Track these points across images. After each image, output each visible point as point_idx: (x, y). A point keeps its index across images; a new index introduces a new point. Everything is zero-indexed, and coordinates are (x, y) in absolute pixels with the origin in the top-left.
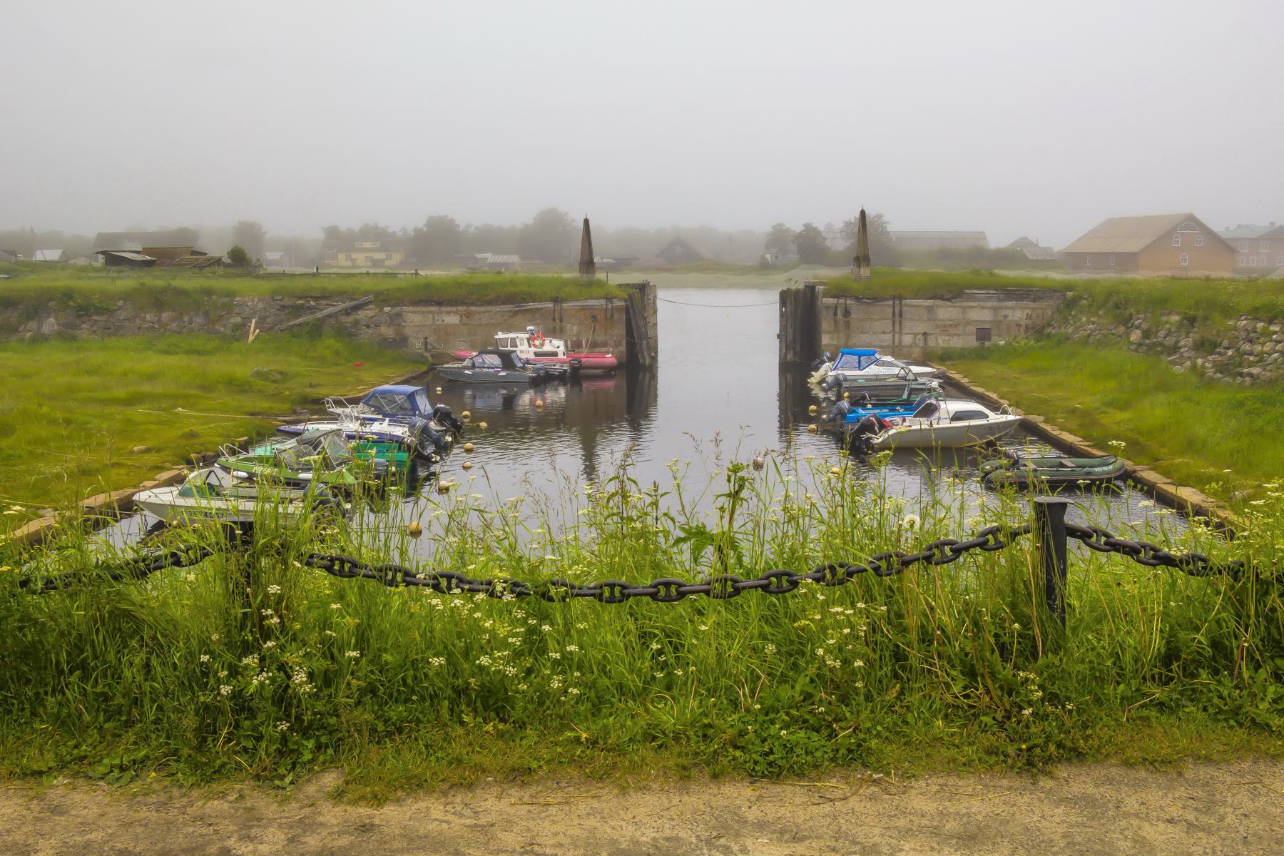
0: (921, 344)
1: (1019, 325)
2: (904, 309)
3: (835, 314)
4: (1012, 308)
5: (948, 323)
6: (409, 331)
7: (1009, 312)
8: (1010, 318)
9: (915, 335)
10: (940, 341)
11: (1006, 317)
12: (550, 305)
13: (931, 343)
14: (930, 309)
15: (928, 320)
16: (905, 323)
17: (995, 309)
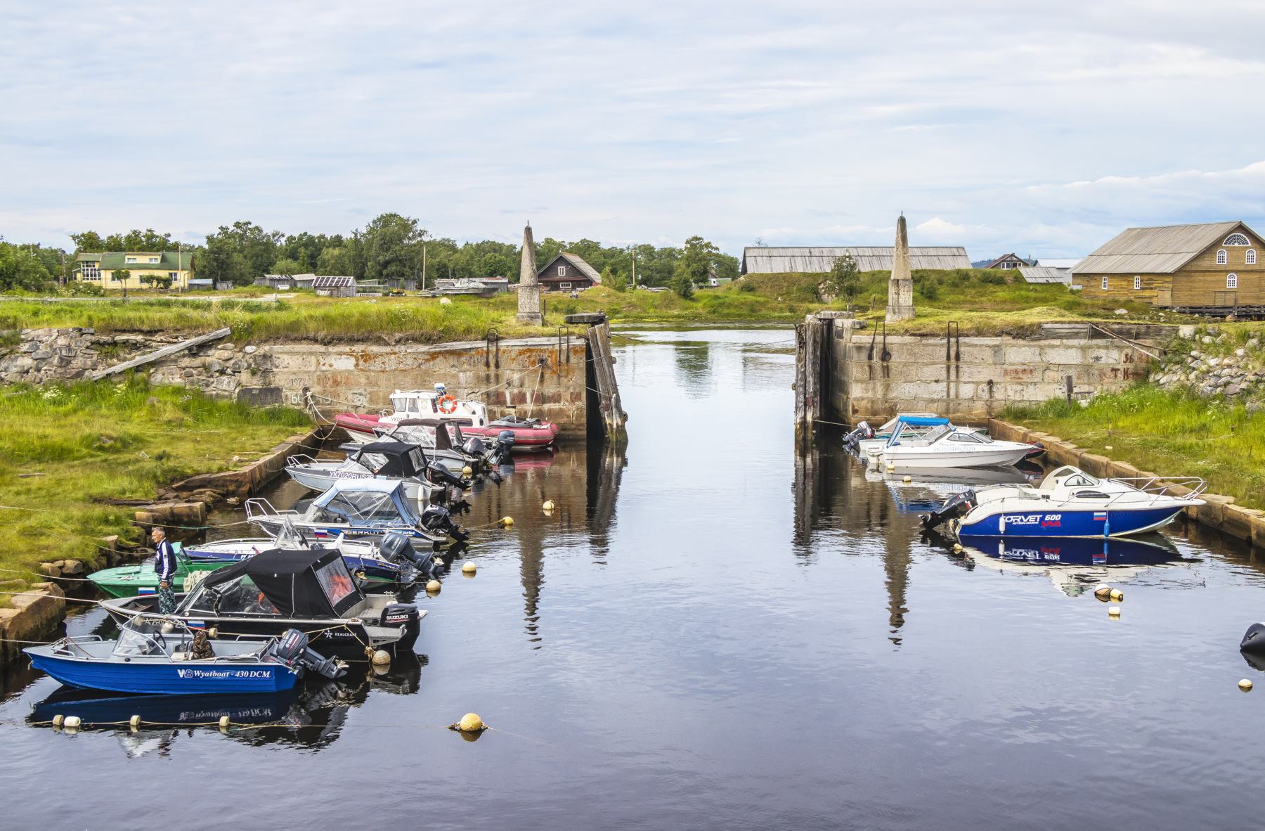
0: (986, 396)
1: (1115, 370)
2: (962, 349)
3: (870, 357)
4: (1107, 347)
5: (1021, 368)
6: (279, 380)
7: (1102, 353)
8: (1103, 361)
9: (977, 383)
10: (1010, 393)
11: (1097, 358)
12: (482, 344)
13: (999, 395)
14: (997, 349)
15: (995, 364)
16: (964, 368)
17: (1083, 349)
